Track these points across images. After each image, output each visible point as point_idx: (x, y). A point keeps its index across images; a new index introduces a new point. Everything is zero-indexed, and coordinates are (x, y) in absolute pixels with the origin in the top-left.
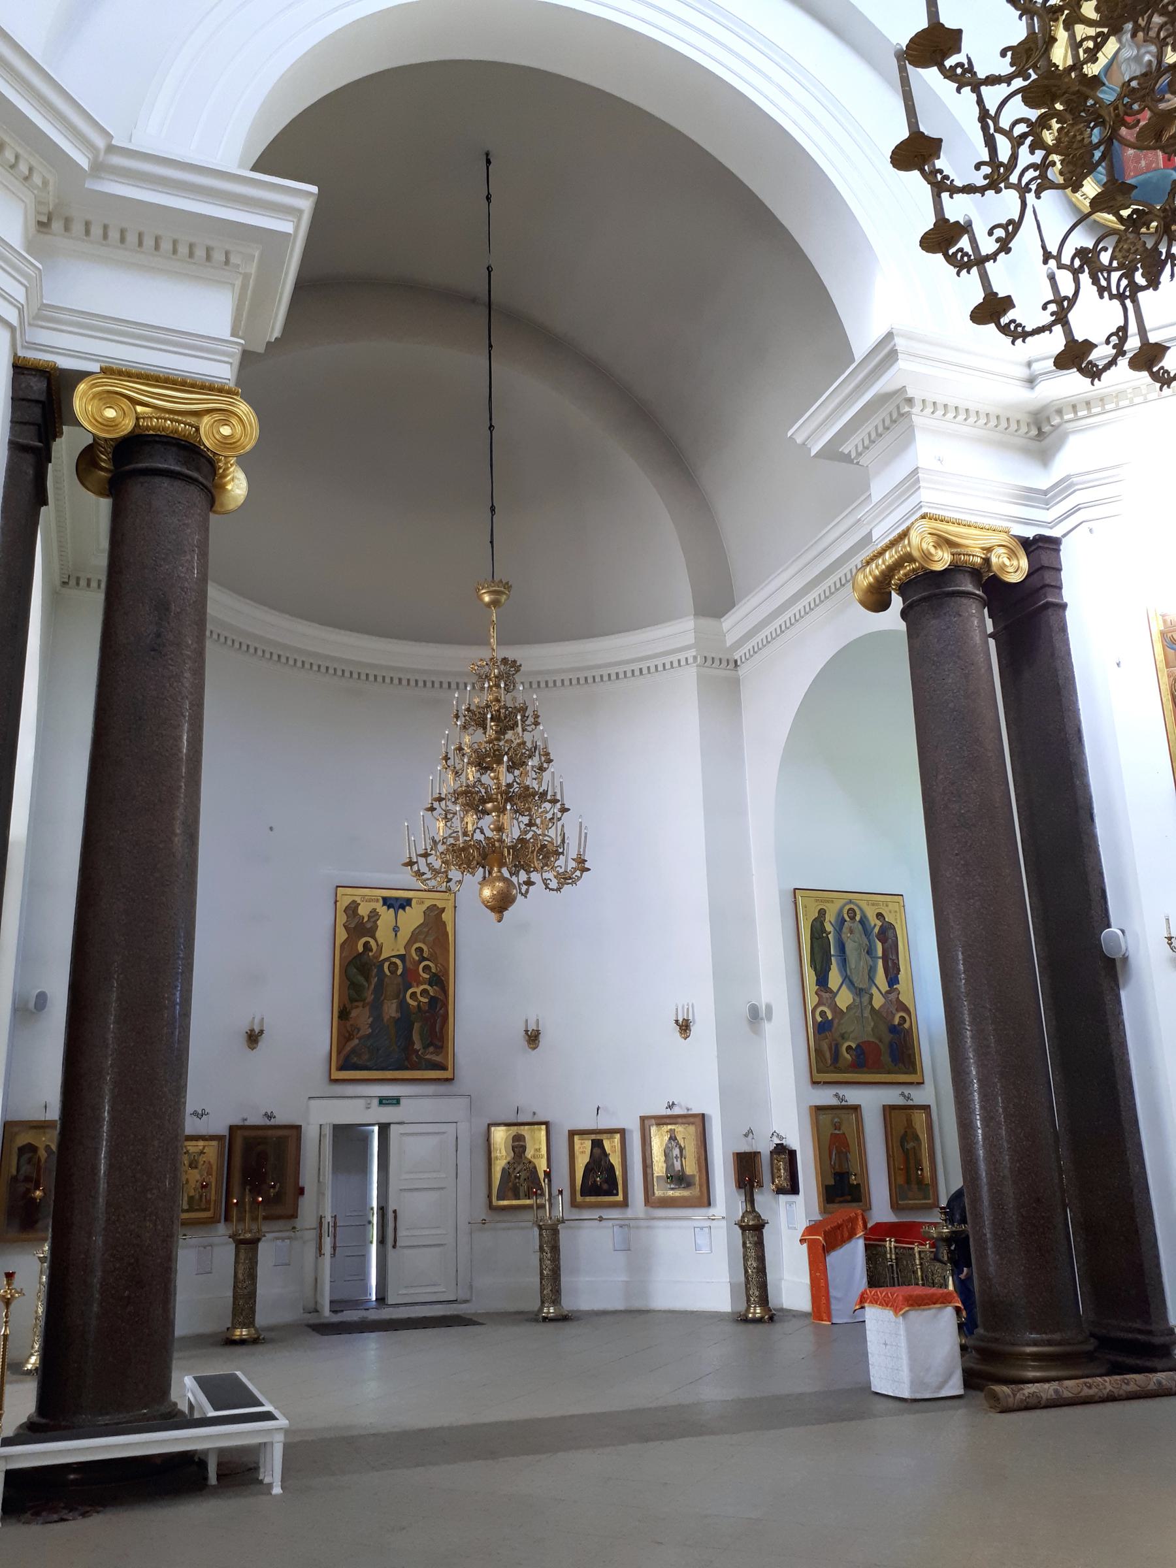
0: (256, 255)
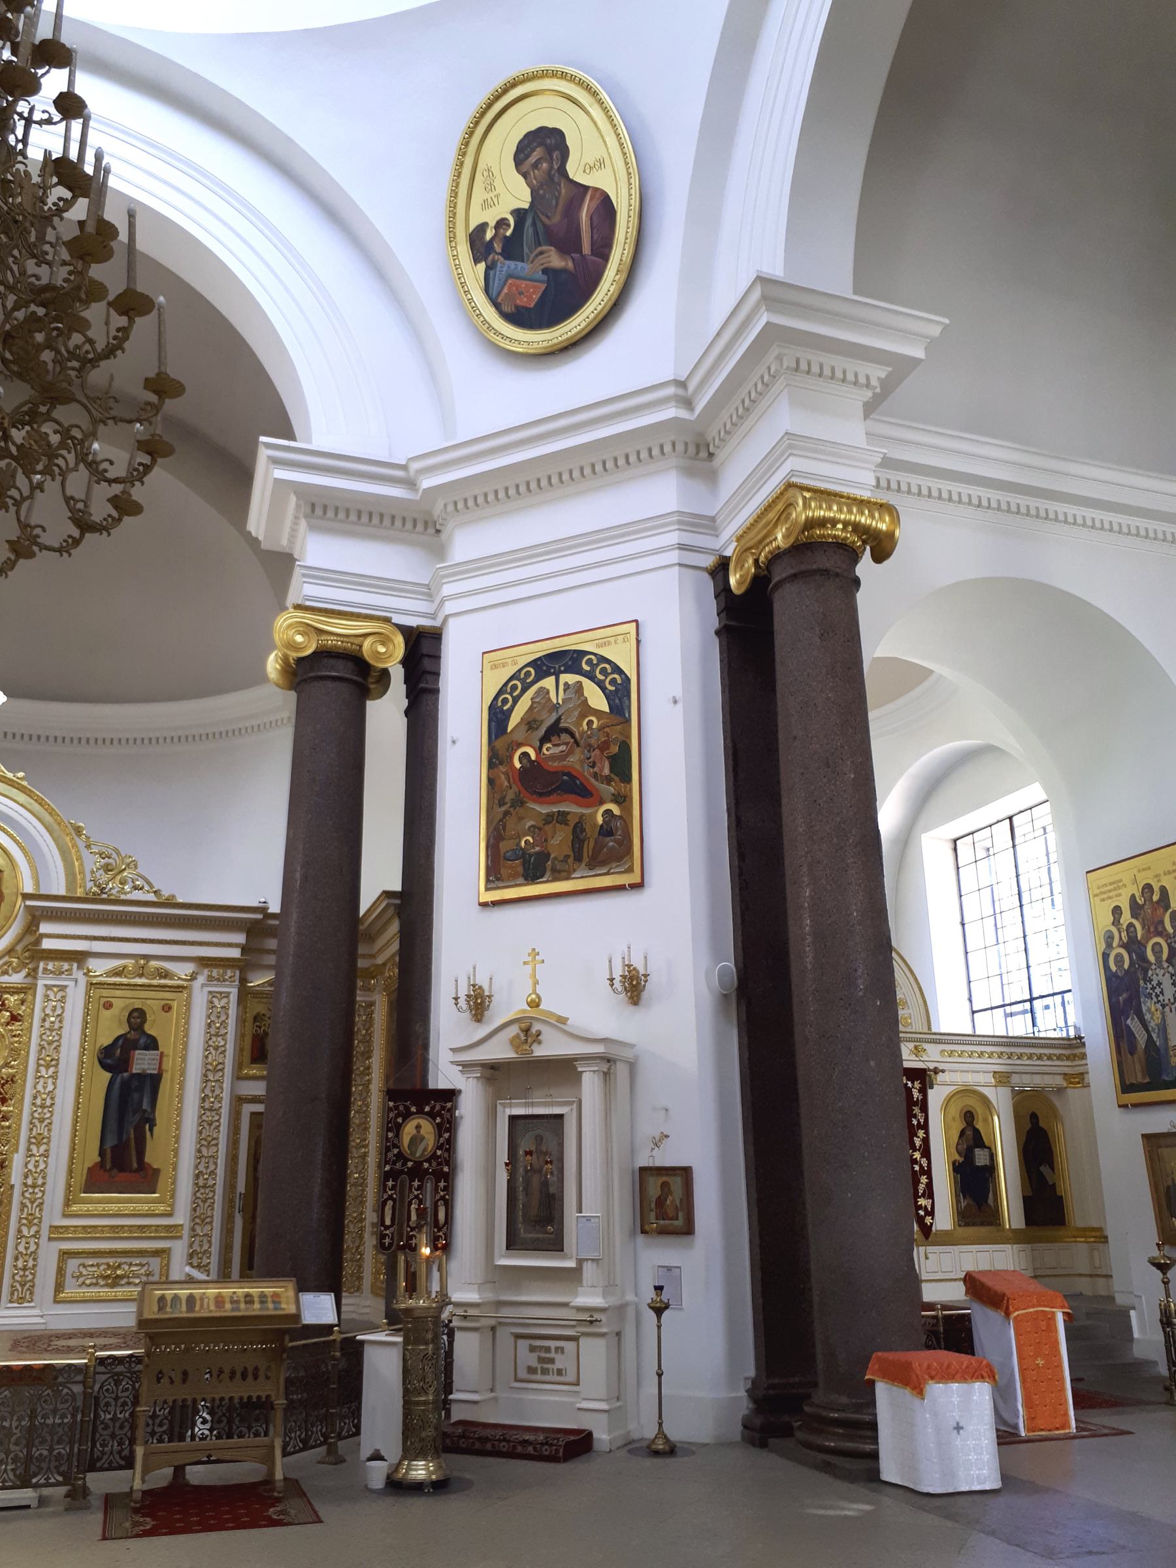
0: (544, 809)
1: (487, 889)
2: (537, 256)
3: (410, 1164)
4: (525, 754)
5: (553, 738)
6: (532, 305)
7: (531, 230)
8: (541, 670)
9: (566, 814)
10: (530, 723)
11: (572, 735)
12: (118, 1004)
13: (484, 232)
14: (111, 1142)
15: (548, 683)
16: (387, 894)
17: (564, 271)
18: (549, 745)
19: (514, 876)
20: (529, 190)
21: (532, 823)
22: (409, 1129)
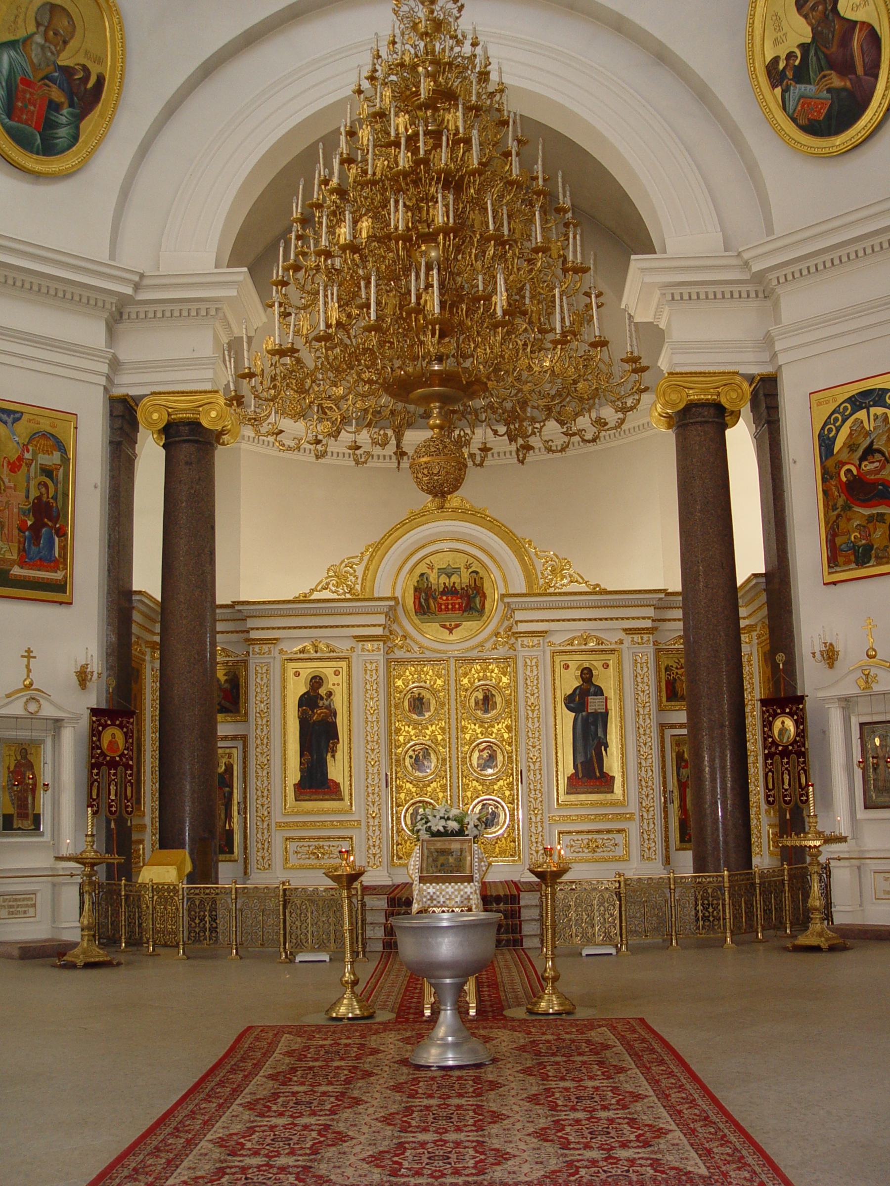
0: (867, 512)
1: (829, 573)
2: (821, 79)
3: (780, 748)
4: (849, 471)
5: (869, 458)
6: (821, 118)
7: (815, 59)
8: (855, 405)
9: (883, 515)
10: (851, 447)
11: (883, 454)
12: (573, 666)
13: (778, 64)
14: (580, 759)
15: (862, 414)
16: (755, 575)
17: (844, 89)
18: (866, 463)
19: (845, 563)
20: (809, 29)
21: (858, 522)
22: (777, 725)
